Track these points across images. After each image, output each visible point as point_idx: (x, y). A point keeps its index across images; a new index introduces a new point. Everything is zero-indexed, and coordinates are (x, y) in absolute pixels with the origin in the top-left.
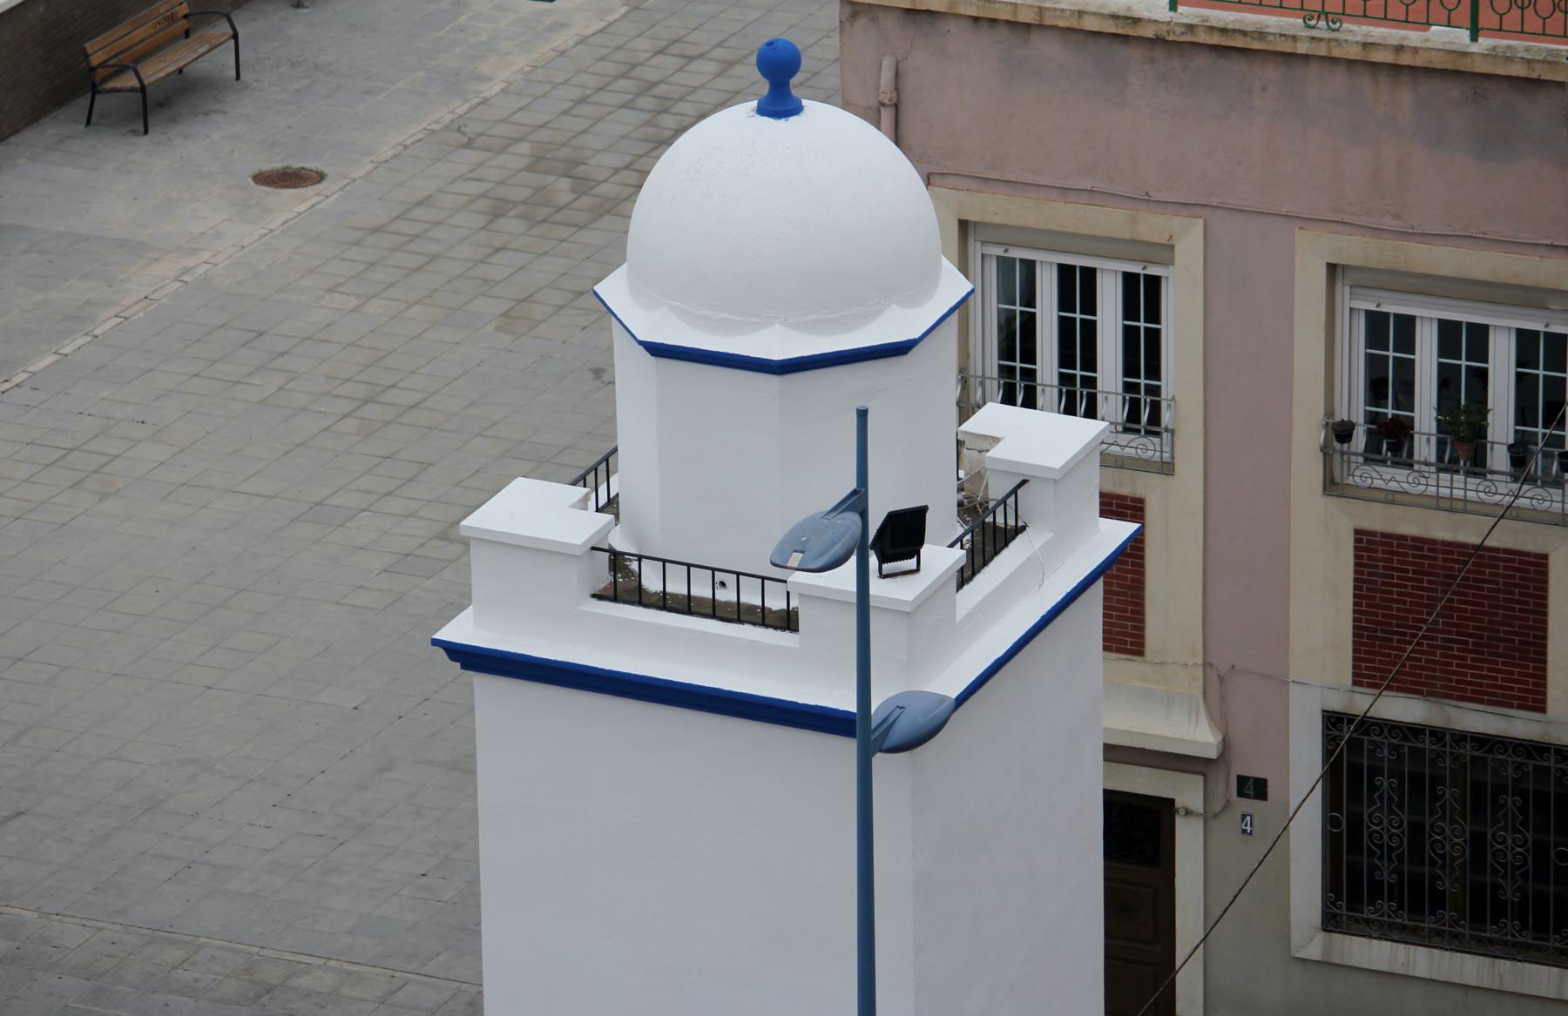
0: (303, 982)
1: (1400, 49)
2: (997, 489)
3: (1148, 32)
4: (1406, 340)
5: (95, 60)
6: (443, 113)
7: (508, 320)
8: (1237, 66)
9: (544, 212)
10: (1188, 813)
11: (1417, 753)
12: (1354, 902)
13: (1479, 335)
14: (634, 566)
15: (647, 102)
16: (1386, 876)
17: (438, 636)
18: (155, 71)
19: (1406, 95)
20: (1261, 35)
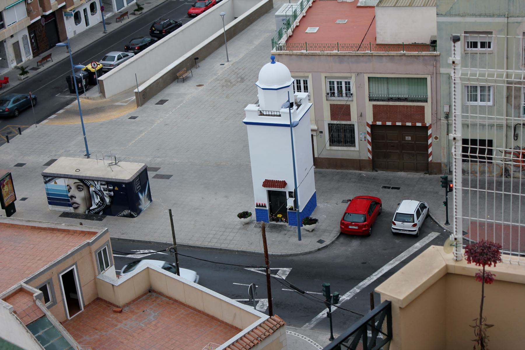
0: (222, 164)
1: (331, 53)
2: (298, 101)
3: (304, 54)
4: (333, 84)
5: (178, 75)
6: (215, 77)
7: (226, 97)
8: (314, 57)
9: (228, 86)
10: (315, 136)
11: (338, 127)
12: (333, 143)
13: (341, 82)
14: (263, 112)
15: (236, 74)
16: (336, 140)
17: (243, 121)
18: (184, 76)
19: (332, 58)
20: (316, 53)
